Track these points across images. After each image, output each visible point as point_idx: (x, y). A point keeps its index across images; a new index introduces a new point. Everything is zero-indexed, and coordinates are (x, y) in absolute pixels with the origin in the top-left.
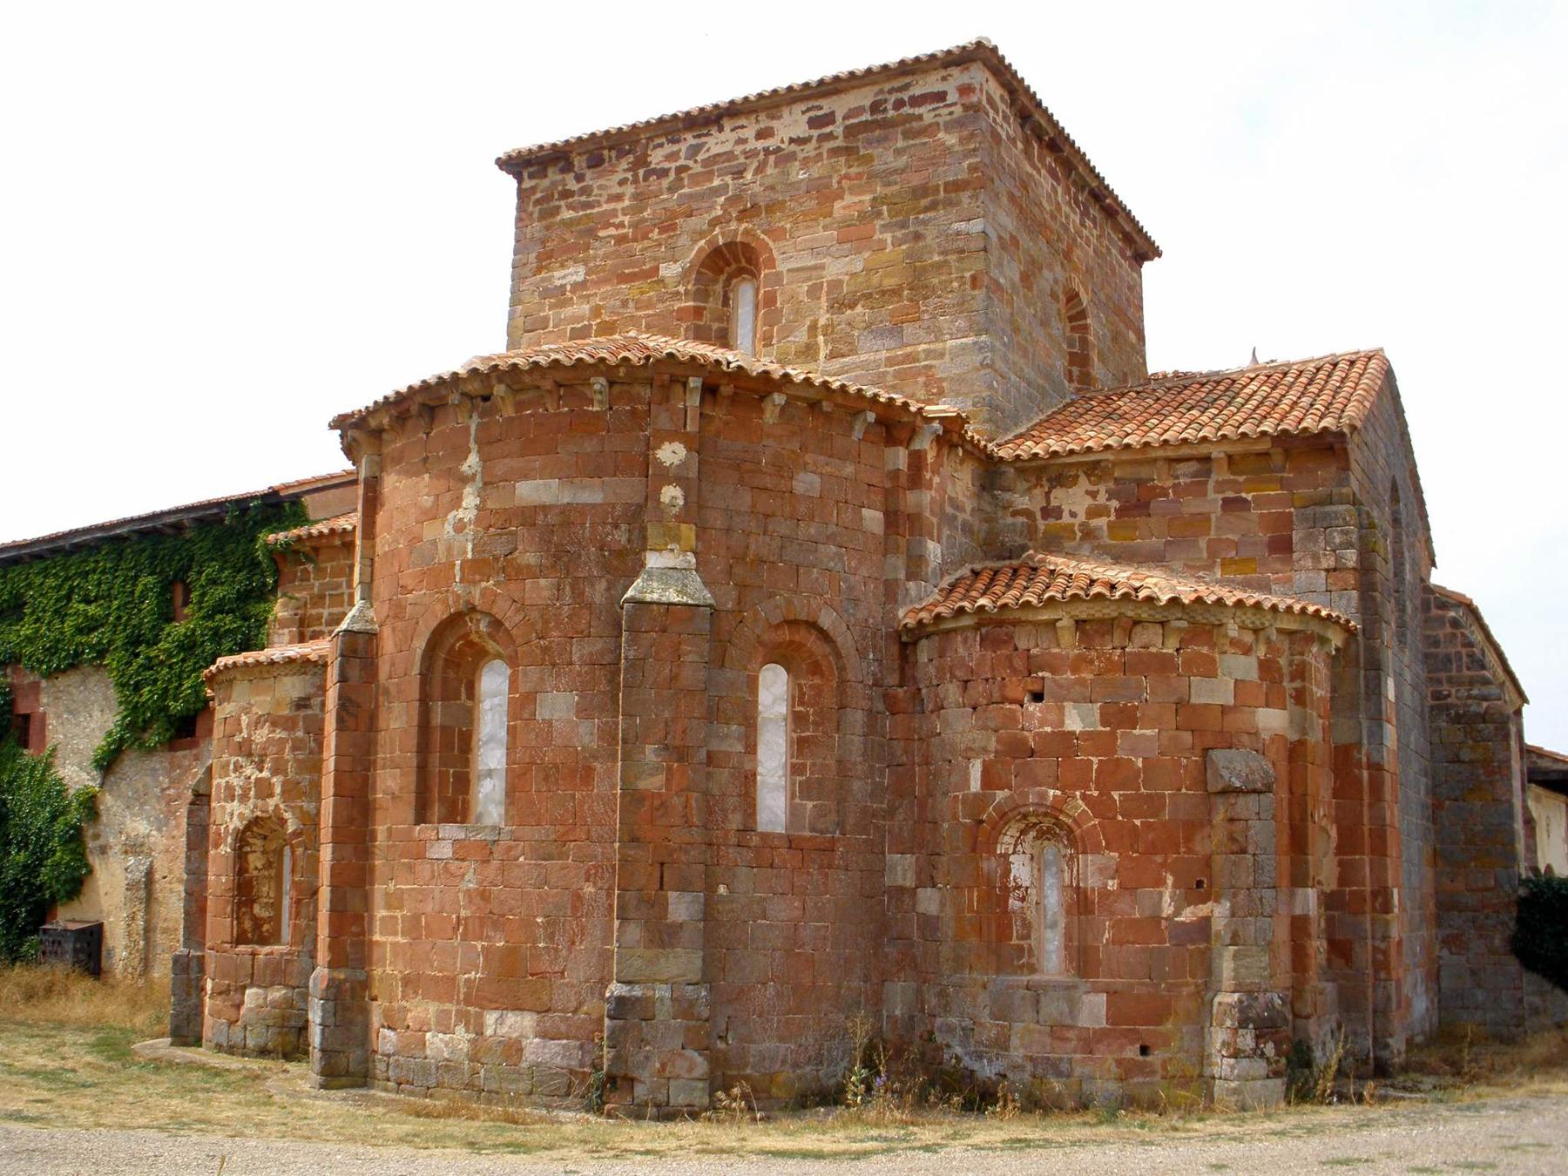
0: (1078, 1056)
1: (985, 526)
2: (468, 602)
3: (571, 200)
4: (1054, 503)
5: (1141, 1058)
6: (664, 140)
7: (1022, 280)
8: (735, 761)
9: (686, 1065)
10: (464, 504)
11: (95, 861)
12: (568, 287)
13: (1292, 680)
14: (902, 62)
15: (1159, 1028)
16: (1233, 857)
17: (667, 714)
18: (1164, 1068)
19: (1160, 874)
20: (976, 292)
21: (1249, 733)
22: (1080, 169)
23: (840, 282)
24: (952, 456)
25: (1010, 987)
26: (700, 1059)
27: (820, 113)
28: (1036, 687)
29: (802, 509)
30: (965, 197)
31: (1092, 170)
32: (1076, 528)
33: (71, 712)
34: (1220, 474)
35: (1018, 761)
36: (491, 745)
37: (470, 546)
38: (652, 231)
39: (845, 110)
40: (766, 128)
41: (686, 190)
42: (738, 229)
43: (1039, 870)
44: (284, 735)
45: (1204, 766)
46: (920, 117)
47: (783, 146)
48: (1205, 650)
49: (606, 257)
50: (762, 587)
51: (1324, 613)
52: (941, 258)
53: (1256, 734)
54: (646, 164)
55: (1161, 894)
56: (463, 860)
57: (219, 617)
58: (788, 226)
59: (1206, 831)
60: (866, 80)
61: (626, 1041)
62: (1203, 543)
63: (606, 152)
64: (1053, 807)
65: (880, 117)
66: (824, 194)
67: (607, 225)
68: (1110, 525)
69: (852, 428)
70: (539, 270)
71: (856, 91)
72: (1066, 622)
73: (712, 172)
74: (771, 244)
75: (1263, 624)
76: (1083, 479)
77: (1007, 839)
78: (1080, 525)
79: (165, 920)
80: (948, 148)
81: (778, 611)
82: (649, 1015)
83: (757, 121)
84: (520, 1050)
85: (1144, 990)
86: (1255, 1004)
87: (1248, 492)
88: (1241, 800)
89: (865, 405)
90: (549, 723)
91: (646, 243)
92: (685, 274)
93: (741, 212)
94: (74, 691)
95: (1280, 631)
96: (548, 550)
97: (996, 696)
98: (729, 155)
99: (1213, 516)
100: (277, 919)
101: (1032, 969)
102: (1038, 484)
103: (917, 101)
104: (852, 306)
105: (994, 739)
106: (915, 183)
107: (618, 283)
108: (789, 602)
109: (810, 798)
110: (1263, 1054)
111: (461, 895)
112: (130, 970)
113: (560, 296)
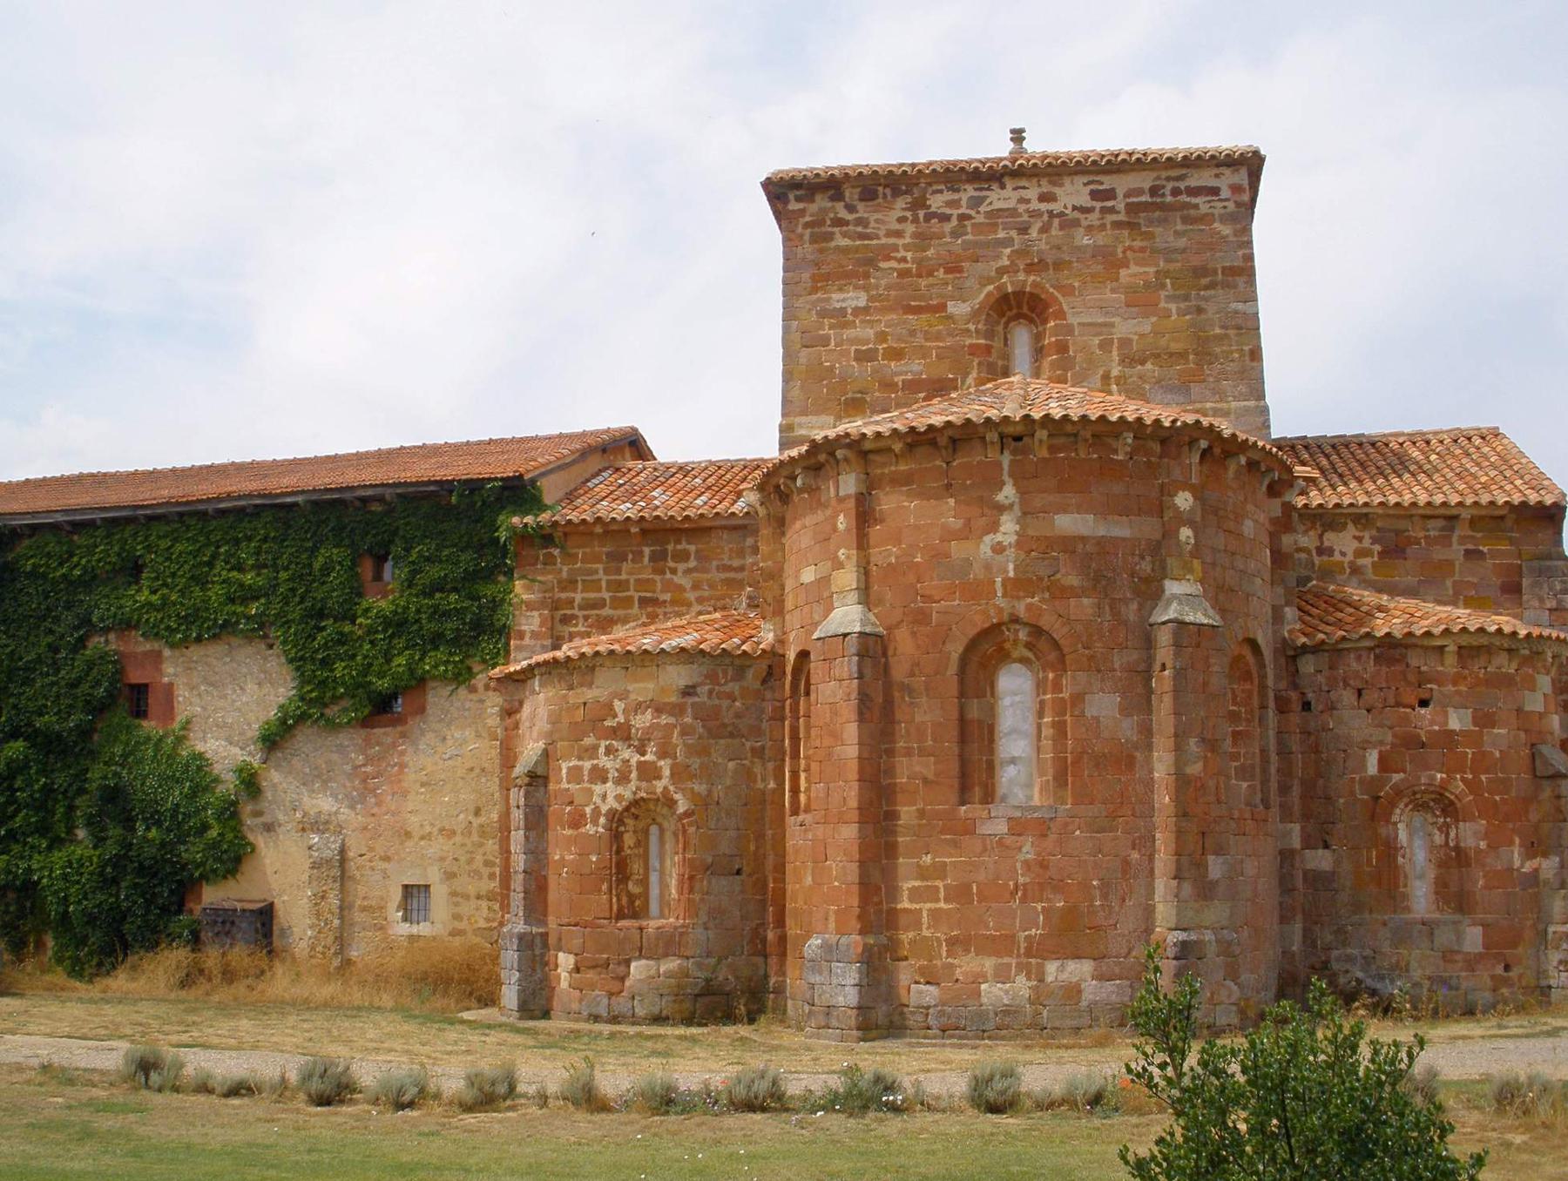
0: (1464, 974)
2: (1012, 614)
3: (845, 228)
4: (1327, 544)
10: (1002, 529)
11: (259, 840)
12: (849, 311)
17: (1202, 713)
18: (1519, 980)
23: (1130, 340)
27: (1101, 188)
28: (1425, 696)
33: (1098, 722)
36: (1014, 736)
37: (1011, 566)
41: (969, 237)
44: (672, 720)
46: (1196, 206)
49: (888, 288)
52: (1223, 331)
54: (925, 206)
55: (1512, 852)
56: (1019, 835)
57: (438, 595)
58: (1076, 284)
62: (1449, 583)
66: (1111, 262)
67: (888, 258)
68: (1374, 564)
70: (815, 290)
72: (1452, 648)
73: (996, 225)
74: (1059, 296)
79: (364, 898)
80: (1223, 237)
84: (1080, 992)
90: (1097, 719)
92: (975, 315)
94: (215, 662)
96: (1089, 574)
97: (1391, 701)
98: (1013, 212)
99: (1457, 563)
100: (645, 895)
102: (1313, 527)
103: (1193, 192)
104: (1143, 363)
107: (905, 313)
109: (1244, 780)
111: (1019, 865)
112: (319, 949)
113: (840, 318)
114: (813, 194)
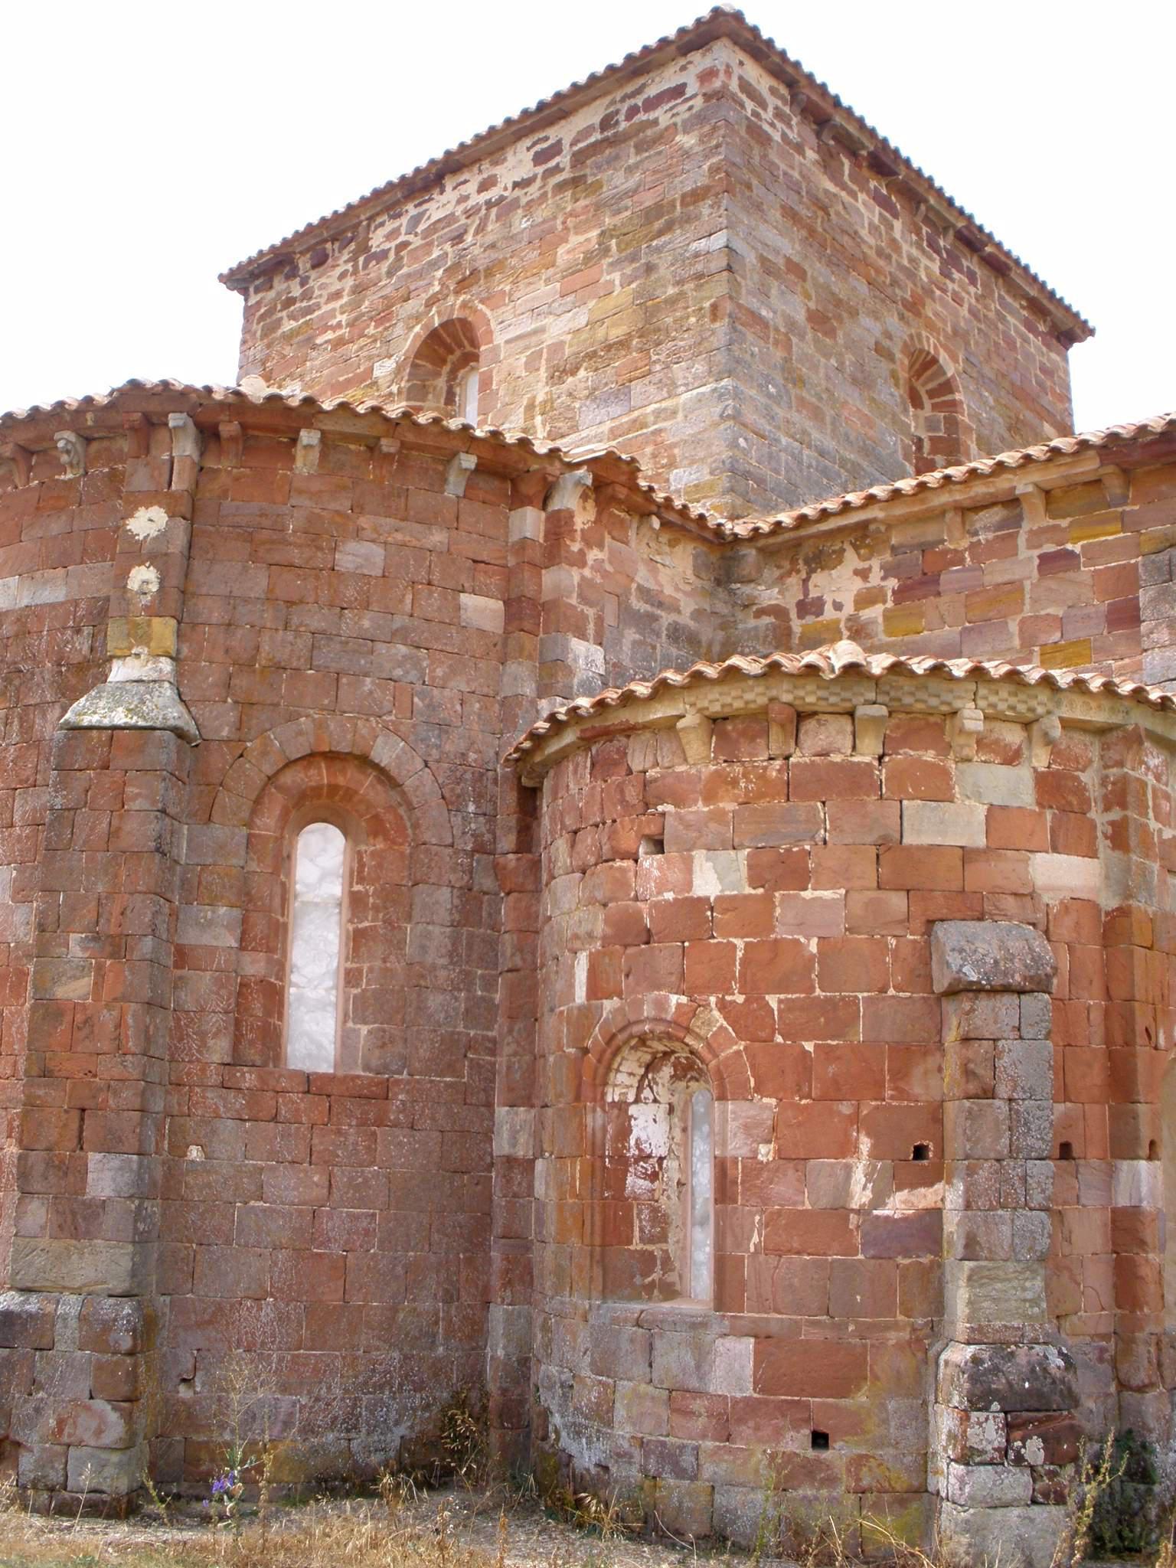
0: (709, 1444)
1: (720, 635)
4: (814, 594)
5: (811, 1453)
6: (385, 217)
7: (1009, 430)
8: (221, 960)
9: (94, 1424)
13: (1107, 809)
14: (630, 58)
15: (843, 1402)
16: (967, 1103)
17: (100, 888)
19: (847, 1135)
20: (717, 325)
21: (1015, 894)
22: (932, 201)
23: (562, 343)
24: (644, 530)
25: (615, 1320)
26: (113, 1417)
27: (545, 145)
28: (652, 829)
29: (350, 593)
30: (705, 209)
31: (950, 202)
32: (842, 625)
34: (1035, 519)
35: (630, 951)
38: (368, 326)
39: (573, 134)
40: (490, 177)
41: (405, 270)
42: (454, 306)
43: (684, 1130)
45: (926, 953)
46: (655, 122)
47: (506, 194)
48: (929, 756)
50: (277, 705)
51: (1154, 695)
53: (1032, 895)
55: (848, 1170)
58: (507, 288)
59: (931, 1062)
60: (593, 92)
61: (10, 1383)
62: (1013, 626)
63: (329, 246)
64: (675, 1023)
65: (609, 133)
66: (546, 239)
67: (326, 328)
68: (887, 616)
69: (444, 481)
71: (585, 109)
72: (690, 720)
74: (488, 312)
75: (1032, 710)
76: (850, 555)
77: (621, 1078)
78: (849, 620)
81: (301, 739)
82: (45, 1342)
83: (480, 171)
85: (814, 1335)
86: (1007, 1367)
87: (1075, 541)
88: (984, 1004)
89: (456, 443)
91: (362, 342)
93: (458, 283)
95: (1067, 724)
98: (450, 219)
99: (1027, 585)
101: (670, 1292)
104: (573, 372)
105: (601, 917)
106: (647, 204)
108: (320, 725)
109: (365, 1023)
110: (1019, 1460)
114: (271, 280)
